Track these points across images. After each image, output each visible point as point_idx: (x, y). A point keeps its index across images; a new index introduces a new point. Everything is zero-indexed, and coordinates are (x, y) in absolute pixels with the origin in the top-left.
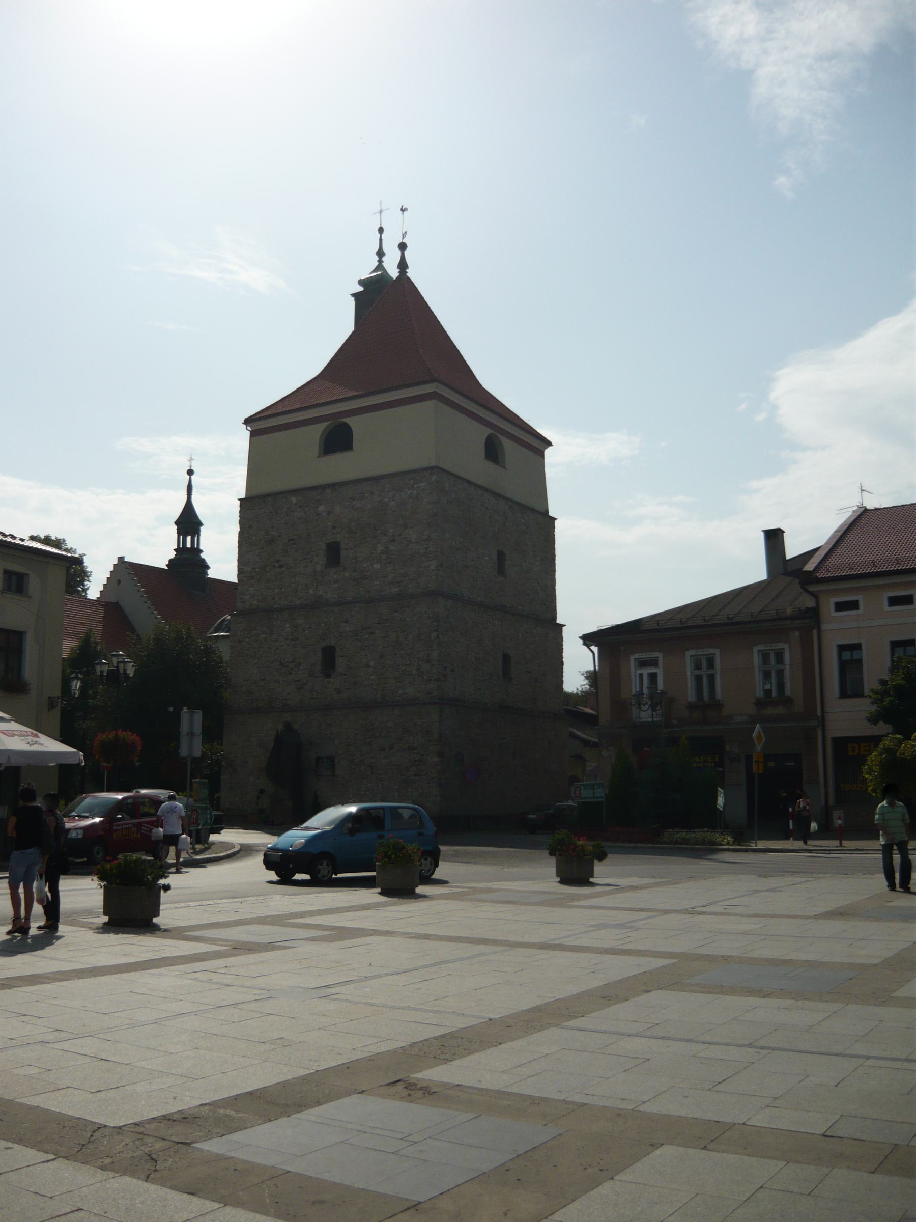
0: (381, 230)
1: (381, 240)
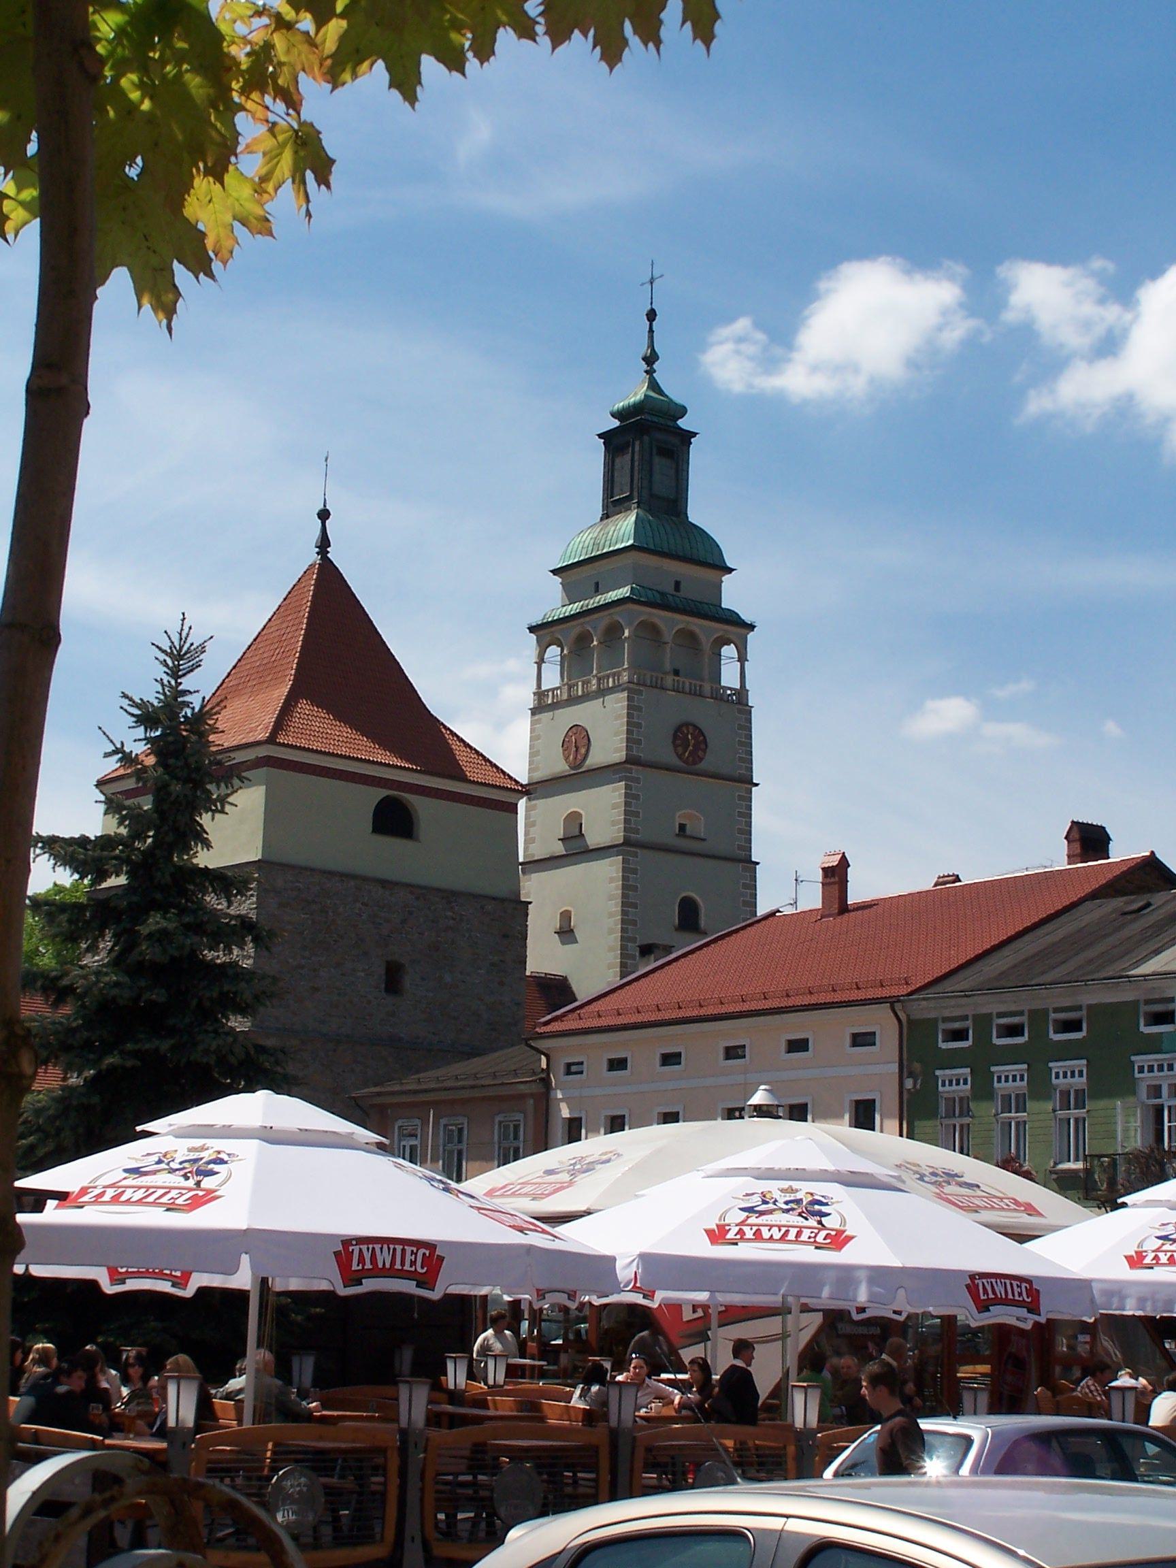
0: (652, 315)
1: (651, 331)
